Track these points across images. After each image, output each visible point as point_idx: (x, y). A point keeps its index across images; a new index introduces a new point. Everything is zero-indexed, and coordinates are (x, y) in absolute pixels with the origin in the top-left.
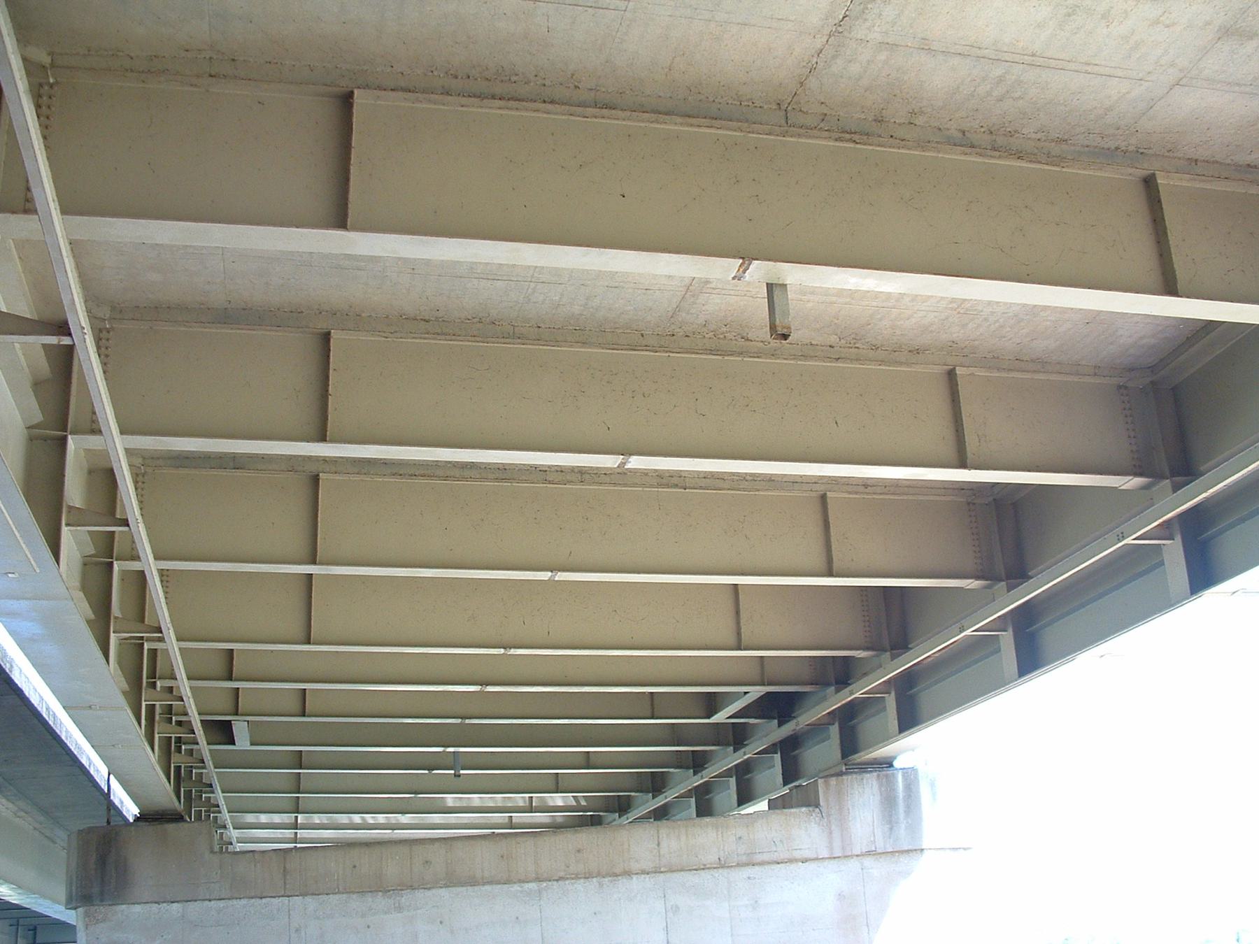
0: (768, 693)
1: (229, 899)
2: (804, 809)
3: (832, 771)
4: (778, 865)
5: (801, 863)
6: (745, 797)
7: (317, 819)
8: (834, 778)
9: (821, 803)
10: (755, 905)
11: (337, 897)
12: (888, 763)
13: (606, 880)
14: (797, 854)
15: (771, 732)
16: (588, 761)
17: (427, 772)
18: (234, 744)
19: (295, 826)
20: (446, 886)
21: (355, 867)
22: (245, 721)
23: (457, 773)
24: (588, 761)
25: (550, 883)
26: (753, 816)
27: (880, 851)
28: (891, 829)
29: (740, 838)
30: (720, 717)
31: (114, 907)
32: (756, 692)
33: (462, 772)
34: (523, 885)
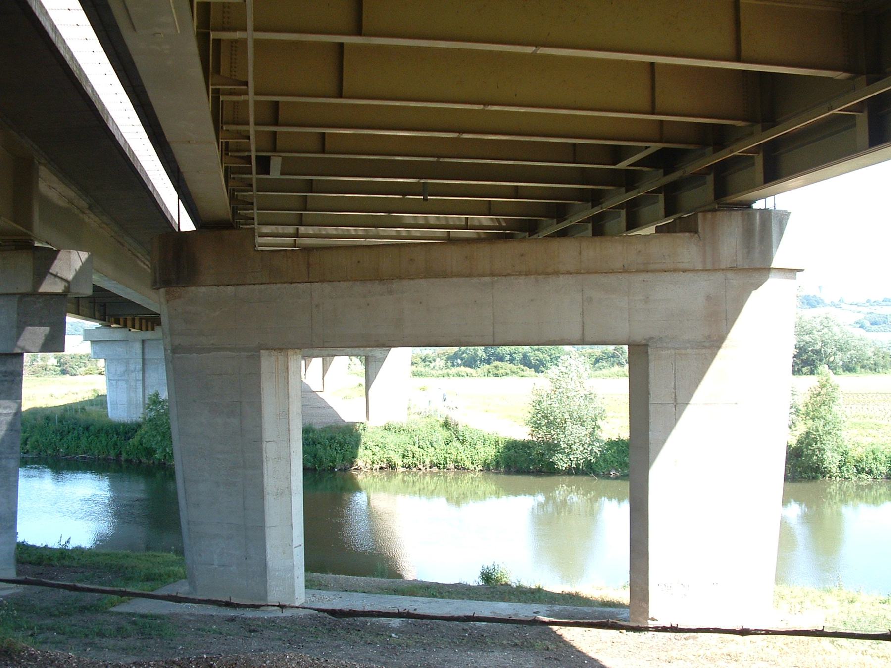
0: (664, 149)
1: (268, 284)
2: (687, 234)
3: (707, 208)
4: (666, 273)
5: (682, 273)
6: (633, 223)
7: (311, 230)
8: (710, 213)
9: (700, 229)
10: (647, 300)
11: (346, 283)
12: (748, 205)
13: (541, 276)
14: (680, 266)
15: (655, 180)
16: (516, 193)
17: (401, 197)
18: (269, 174)
19: (297, 235)
20: (425, 277)
21: (359, 262)
22: (280, 156)
23: (425, 198)
24: (516, 193)
25: (500, 277)
26: (650, 236)
27: (740, 267)
28: (749, 252)
29: (639, 252)
30: (622, 165)
31: (186, 288)
32: (655, 147)
33: (429, 198)
34: (480, 278)
